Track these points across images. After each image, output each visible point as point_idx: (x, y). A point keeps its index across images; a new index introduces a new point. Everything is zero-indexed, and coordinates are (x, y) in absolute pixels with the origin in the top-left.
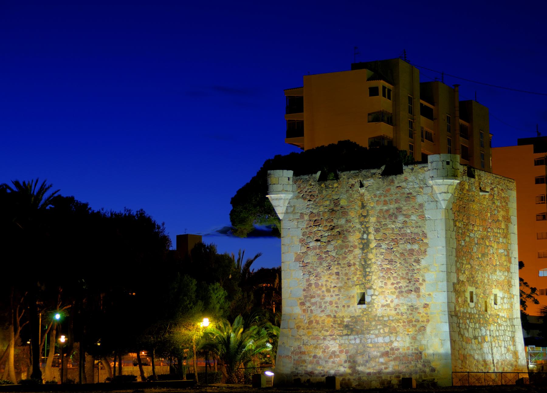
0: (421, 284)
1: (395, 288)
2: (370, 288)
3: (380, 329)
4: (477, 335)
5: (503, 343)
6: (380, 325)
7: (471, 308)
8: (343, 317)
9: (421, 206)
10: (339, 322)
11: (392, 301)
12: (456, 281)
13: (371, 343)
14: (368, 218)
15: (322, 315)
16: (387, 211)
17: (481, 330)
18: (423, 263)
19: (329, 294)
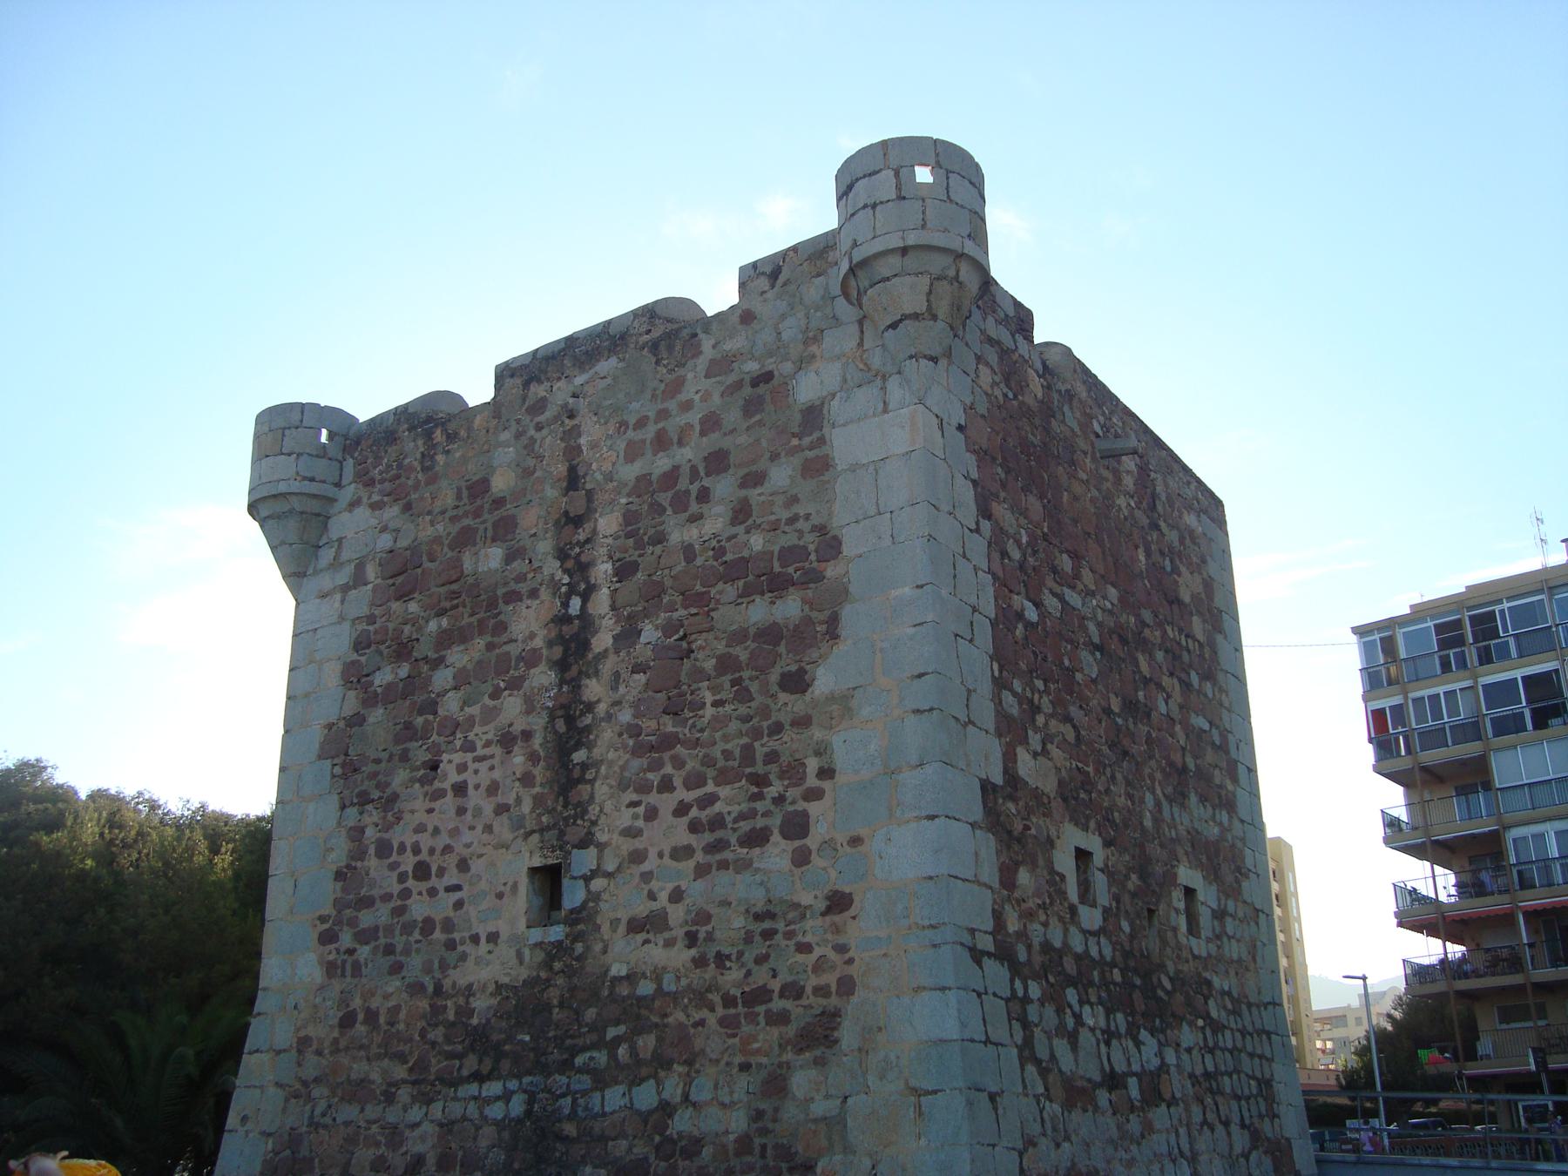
0: (814, 795)
1: (694, 827)
2: (583, 844)
3: (617, 1041)
4: (1120, 1067)
5: (1234, 1104)
6: (617, 1023)
7: (1086, 933)
8: (469, 991)
9: (813, 416)
10: (451, 1016)
11: (677, 896)
12: (998, 779)
13: (573, 1116)
14: (588, 526)
15: (394, 984)
16: (671, 477)
17: (1138, 1044)
18: (824, 681)
19: (423, 886)
